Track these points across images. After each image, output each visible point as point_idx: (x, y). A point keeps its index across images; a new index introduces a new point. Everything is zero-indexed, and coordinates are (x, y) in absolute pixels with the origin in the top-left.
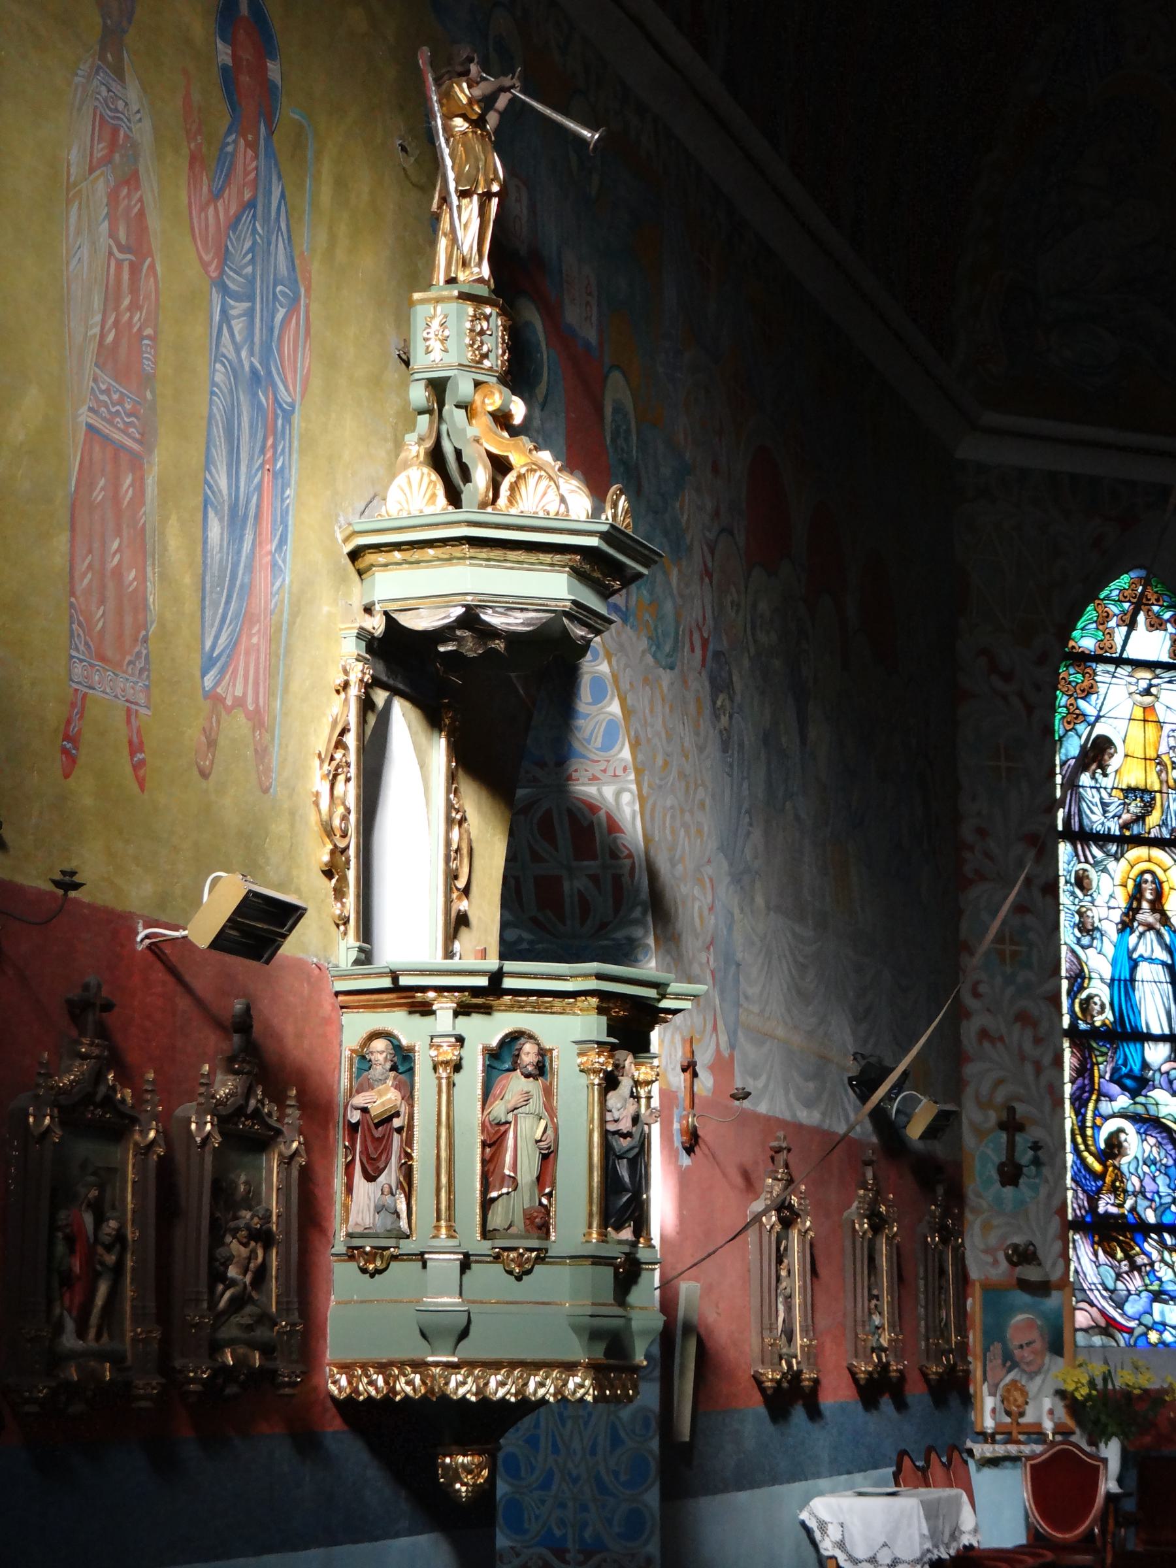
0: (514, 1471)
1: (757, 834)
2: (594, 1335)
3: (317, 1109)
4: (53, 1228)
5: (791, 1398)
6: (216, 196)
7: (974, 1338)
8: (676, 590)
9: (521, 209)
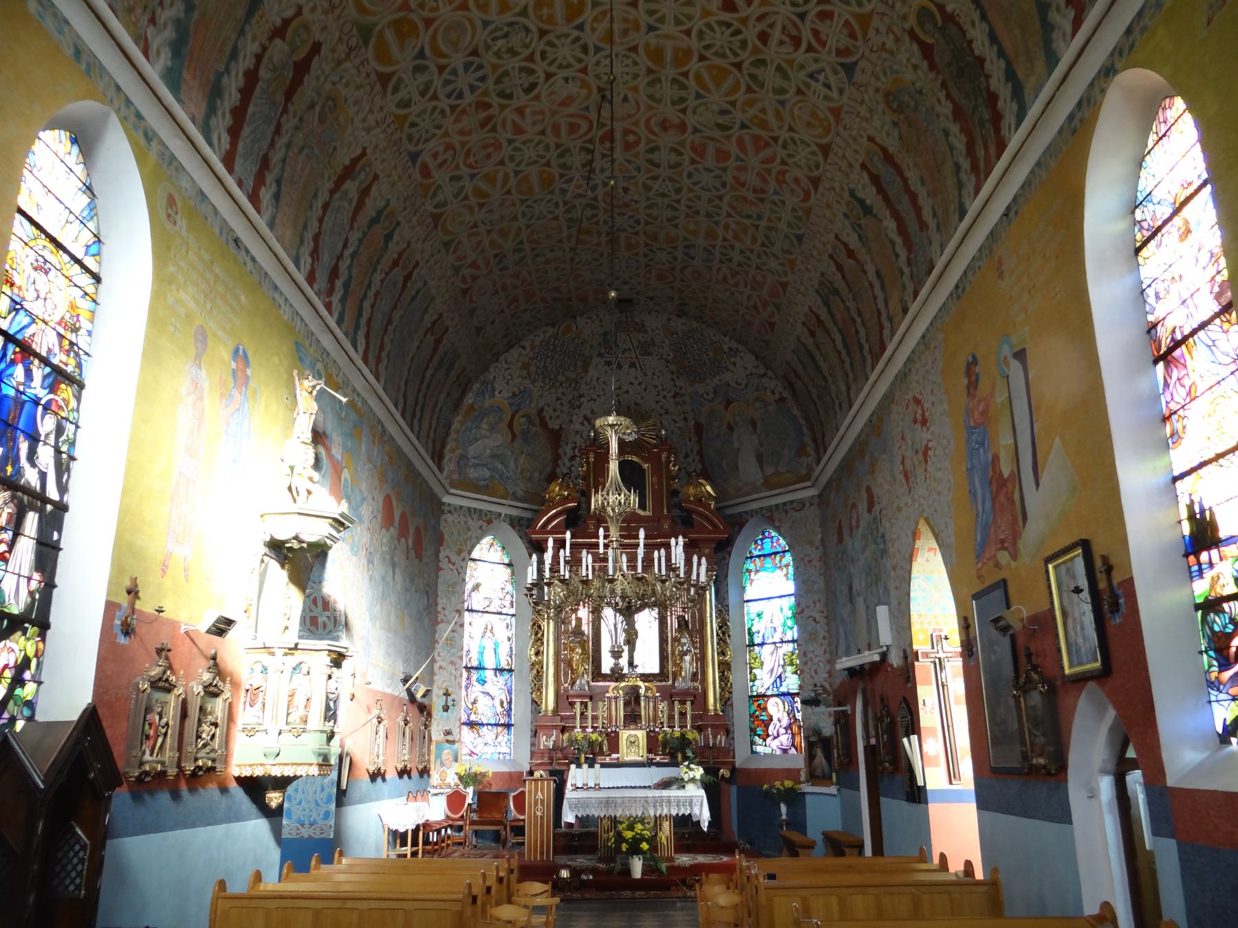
0: (290, 800)
1: (378, 607)
2: (320, 755)
3: (235, 685)
4: (145, 720)
5: (377, 775)
6: (227, 406)
7: (432, 758)
8: (360, 534)
9: (321, 419)
